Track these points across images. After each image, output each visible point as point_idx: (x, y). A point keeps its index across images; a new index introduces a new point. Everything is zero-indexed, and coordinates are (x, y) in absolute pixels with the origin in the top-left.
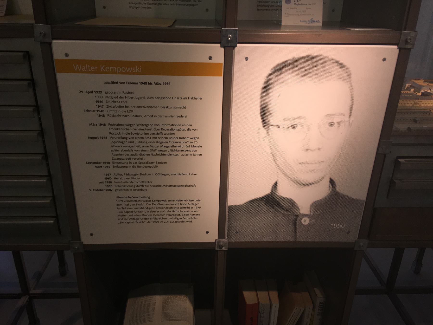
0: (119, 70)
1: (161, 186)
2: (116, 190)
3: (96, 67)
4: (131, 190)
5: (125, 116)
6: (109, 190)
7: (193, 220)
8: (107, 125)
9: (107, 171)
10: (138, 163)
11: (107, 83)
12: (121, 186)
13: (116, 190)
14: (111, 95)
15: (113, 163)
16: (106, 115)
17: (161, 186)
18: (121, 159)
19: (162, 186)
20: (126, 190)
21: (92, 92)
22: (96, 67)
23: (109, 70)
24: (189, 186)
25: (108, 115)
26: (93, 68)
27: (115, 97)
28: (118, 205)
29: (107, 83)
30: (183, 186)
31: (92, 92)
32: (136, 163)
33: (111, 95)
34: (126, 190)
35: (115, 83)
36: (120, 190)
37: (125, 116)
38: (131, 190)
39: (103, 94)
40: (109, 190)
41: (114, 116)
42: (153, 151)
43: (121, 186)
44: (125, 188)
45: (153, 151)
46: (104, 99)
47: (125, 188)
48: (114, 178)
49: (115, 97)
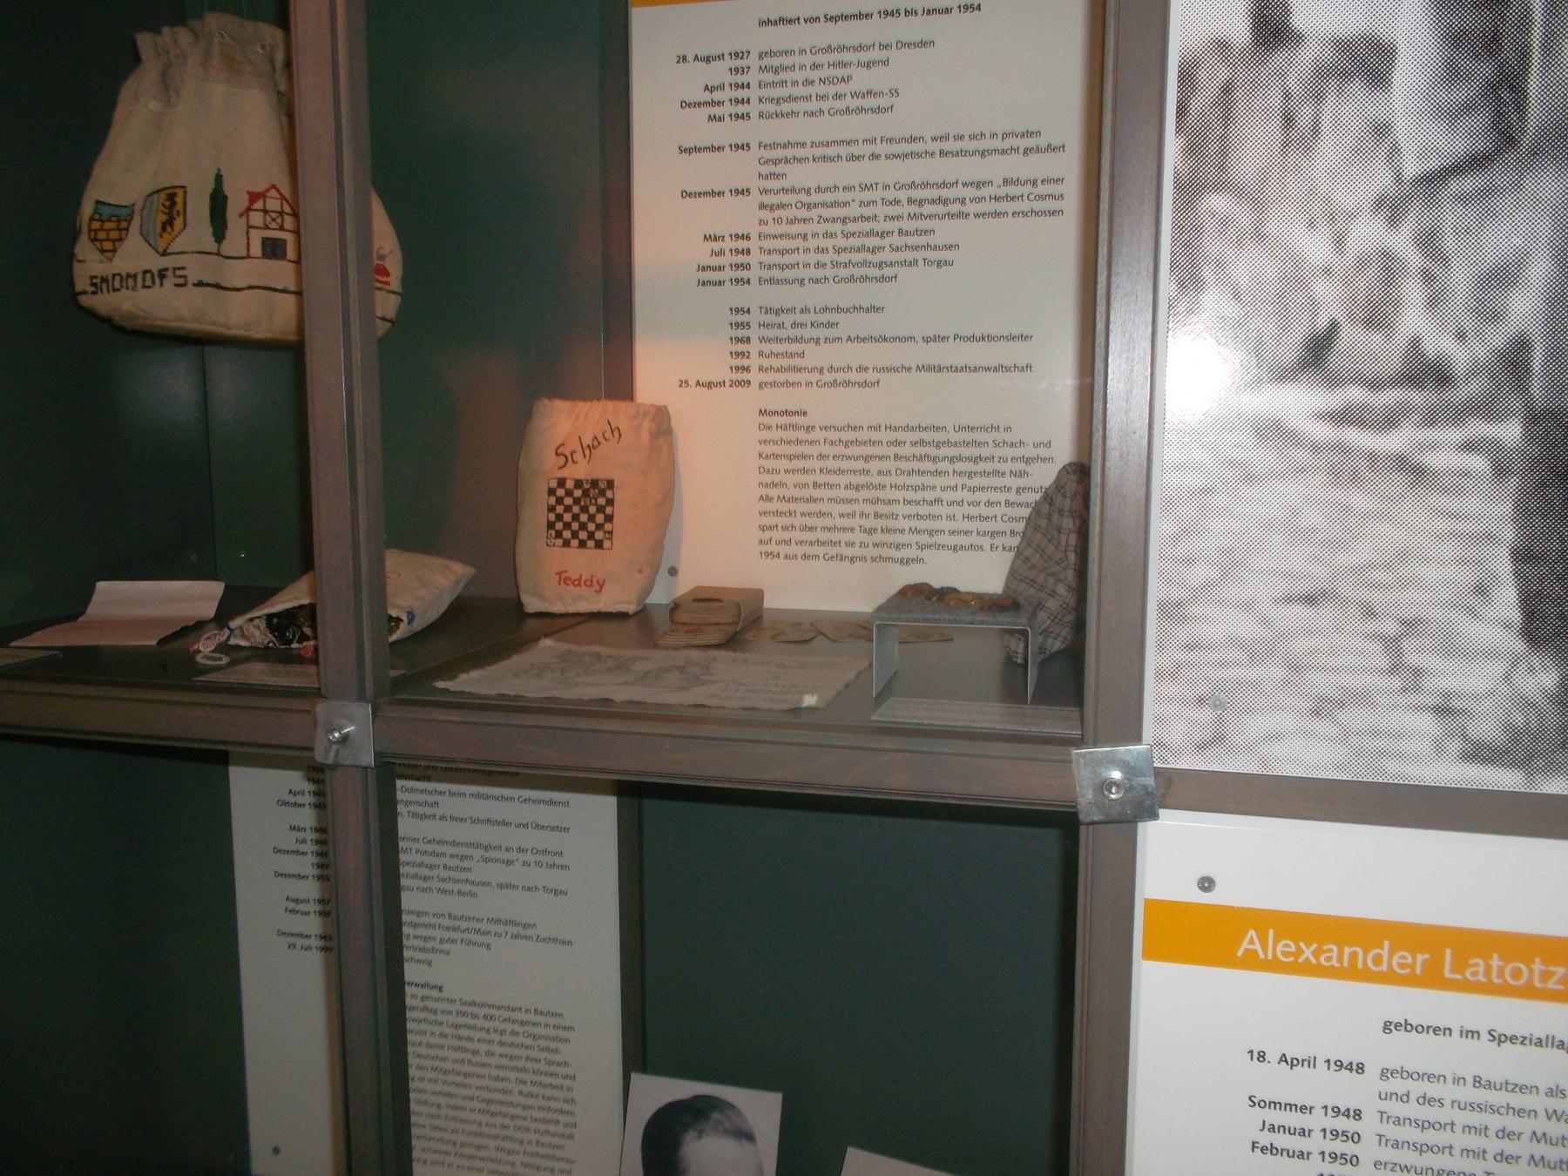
0: (1377, 960)
1: (909, 369)
2: (762, 385)
3: (1420, 958)
4: (809, 384)
5: (812, 114)
6: (740, 383)
7: (903, 272)
8: (754, 146)
9: (740, 295)
10: (831, 250)
11: (768, 22)
12: (779, 370)
13: (762, 385)
14: (775, 61)
15: (760, 236)
16: (754, 115)
17: (909, 369)
18: (778, 101)
19: (914, 367)
20: (792, 384)
21: (721, 57)
22: (1420, 958)
23: (1412, 966)
24: (1008, 369)
25: (761, 115)
26: (1287, 946)
27: (786, 69)
28: (763, 528)
29: (768, 22)
30: (988, 369)
31: (721, 57)
32: (824, 251)
33: (775, 61)
34: (792, 384)
35: (790, 21)
36: (774, 384)
37: (812, 114)
38: (809, 384)
39: (753, 61)
40: (740, 383)
41: (777, 116)
42: (869, 190)
43: (779, 370)
44: (792, 377)
45: (869, 190)
46: (753, 77)
47: (792, 377)
48: (760, 325)
49: (786, 69)
